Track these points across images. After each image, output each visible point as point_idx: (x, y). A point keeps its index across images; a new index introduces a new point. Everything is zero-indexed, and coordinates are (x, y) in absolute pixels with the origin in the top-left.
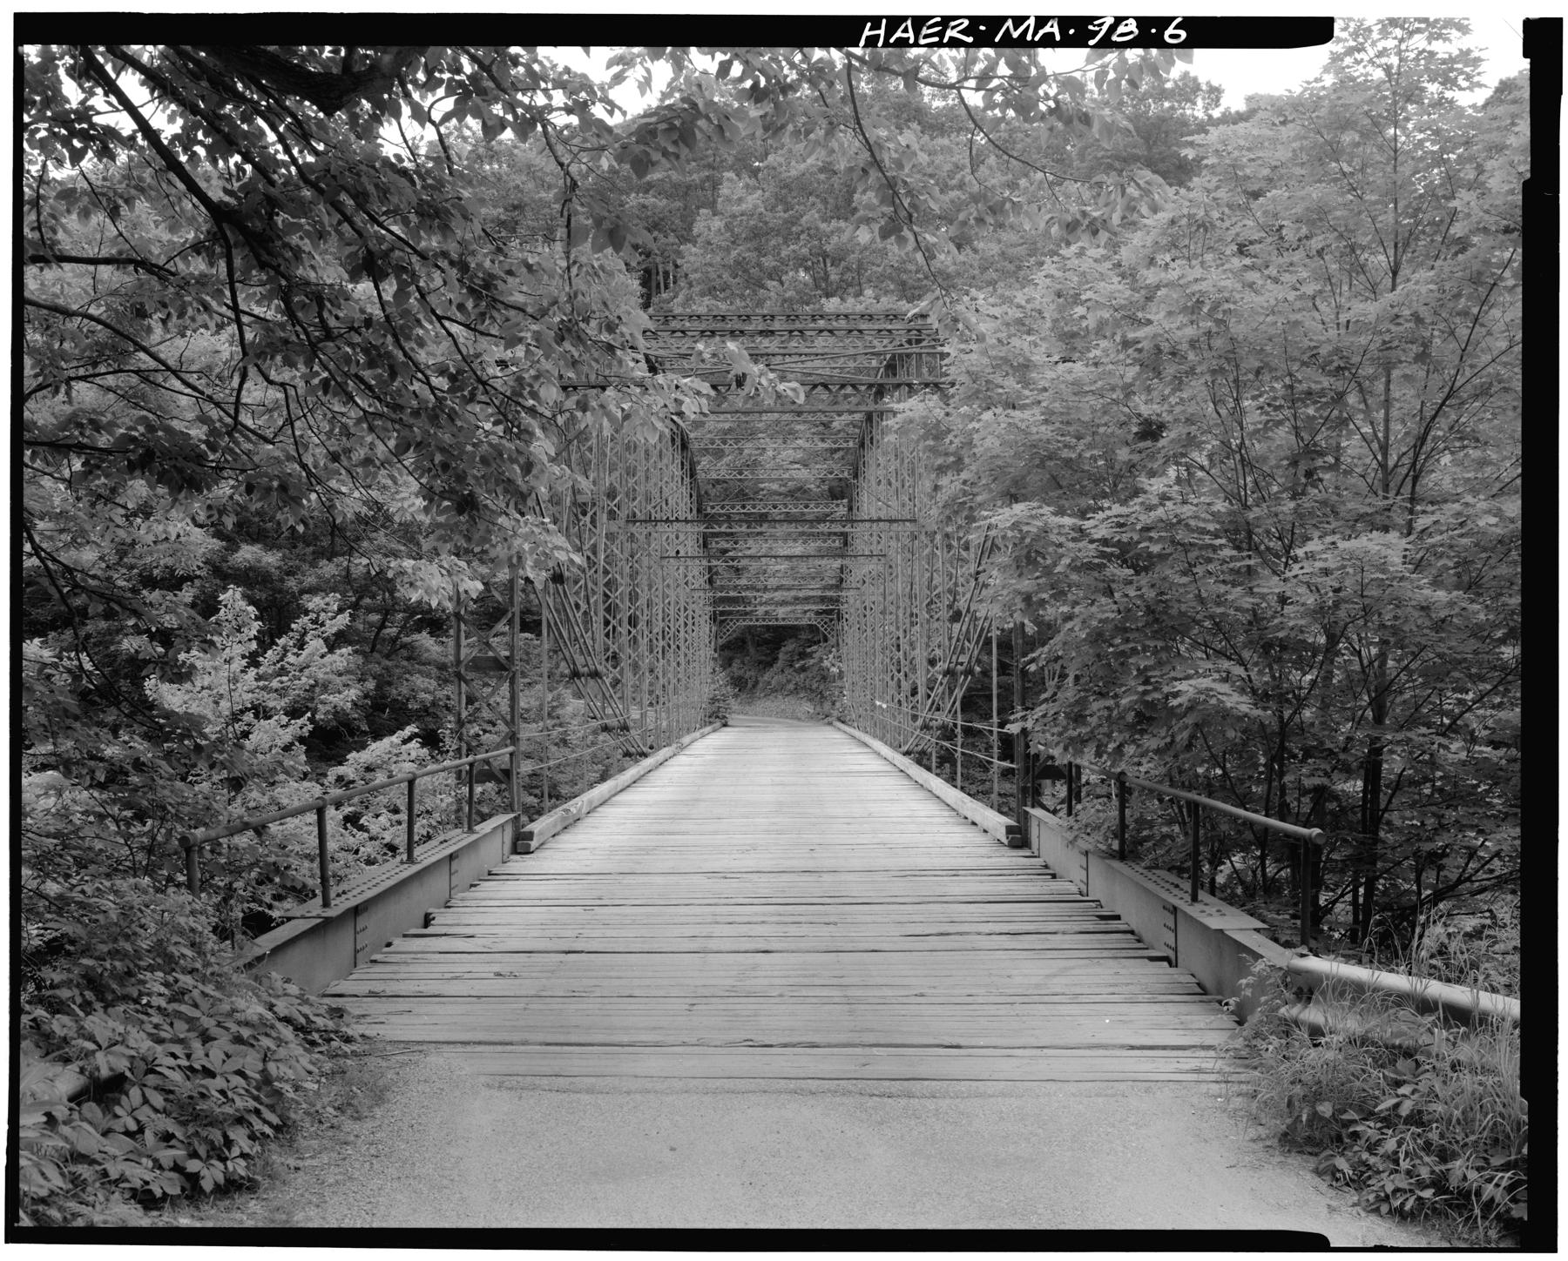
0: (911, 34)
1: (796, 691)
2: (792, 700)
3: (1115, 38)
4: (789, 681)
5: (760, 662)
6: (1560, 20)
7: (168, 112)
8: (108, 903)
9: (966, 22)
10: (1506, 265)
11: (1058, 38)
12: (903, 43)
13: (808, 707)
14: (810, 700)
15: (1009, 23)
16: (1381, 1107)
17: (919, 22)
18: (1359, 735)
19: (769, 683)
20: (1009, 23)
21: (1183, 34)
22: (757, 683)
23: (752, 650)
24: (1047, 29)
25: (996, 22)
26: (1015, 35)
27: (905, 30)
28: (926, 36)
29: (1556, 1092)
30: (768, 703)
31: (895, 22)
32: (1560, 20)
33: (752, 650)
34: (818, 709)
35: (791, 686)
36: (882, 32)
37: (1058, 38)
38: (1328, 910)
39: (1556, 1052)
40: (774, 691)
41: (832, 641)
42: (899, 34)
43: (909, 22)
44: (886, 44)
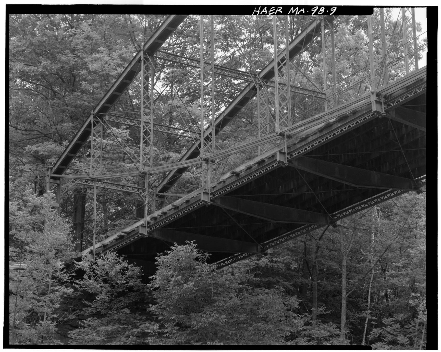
0: (266, 11)
7: (13, 64)
10: (423, 288)
11: (304, 12)
12: (264, 13)
15: (292, 8)
16: (240, 70)
17: (269, 7)
18: (419, 255)
20: (292, 8)
27: (265, 10)
29: (437, 297)
31: (263, 7)
36: (259, 11)
37: (304, 12)
38: (390, 43)
39: (437, 294)
42: (263, 11)
43: (266, 8)
44: (259, 14)
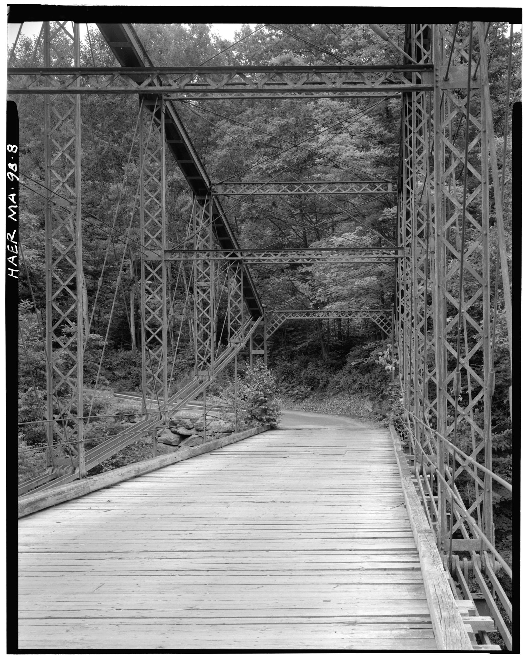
1: (361, 389)
2: (356, 398)
3: (16, 170)
4: (355, 382)
5: (332, 365)
6: (8, 653)
8: (310, 336)
9: (8, 234)
11: (15, 195)
13: (368, 406)
14: (372, 399)
15: (10, 216)
19: (338, 383)
20: (10, 216)
21: (12, 180)
22: (328, 382)
23: (325, 355)
24: (13, 200)
25: (8, 221)
26: (15, 213)
28: (15, 250)
30: (336, 401)
32: (8, 653)
33: (325, 355)
34: (377, 409)
35: (356, 386)
36: (13, 270)
40: (342, 390)
41: (391, 335)
